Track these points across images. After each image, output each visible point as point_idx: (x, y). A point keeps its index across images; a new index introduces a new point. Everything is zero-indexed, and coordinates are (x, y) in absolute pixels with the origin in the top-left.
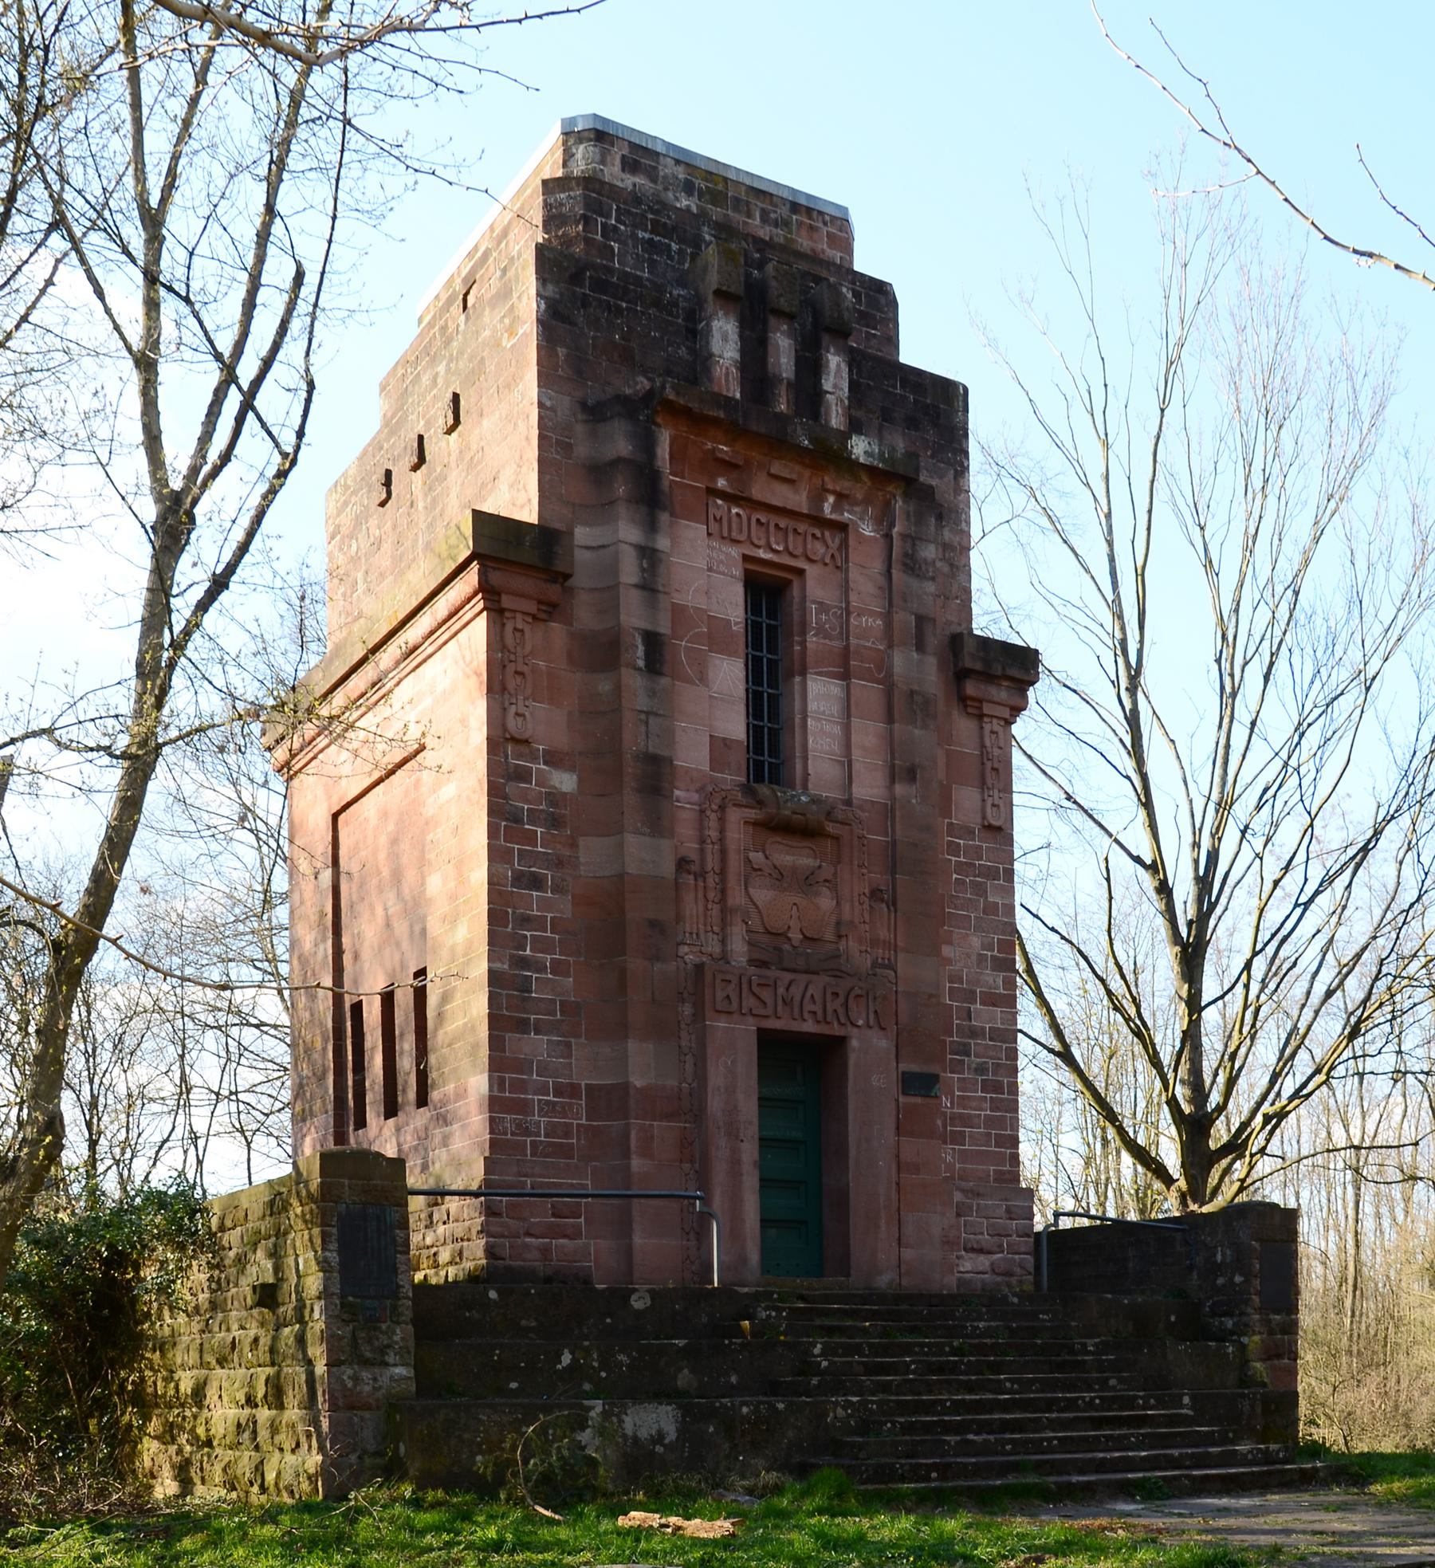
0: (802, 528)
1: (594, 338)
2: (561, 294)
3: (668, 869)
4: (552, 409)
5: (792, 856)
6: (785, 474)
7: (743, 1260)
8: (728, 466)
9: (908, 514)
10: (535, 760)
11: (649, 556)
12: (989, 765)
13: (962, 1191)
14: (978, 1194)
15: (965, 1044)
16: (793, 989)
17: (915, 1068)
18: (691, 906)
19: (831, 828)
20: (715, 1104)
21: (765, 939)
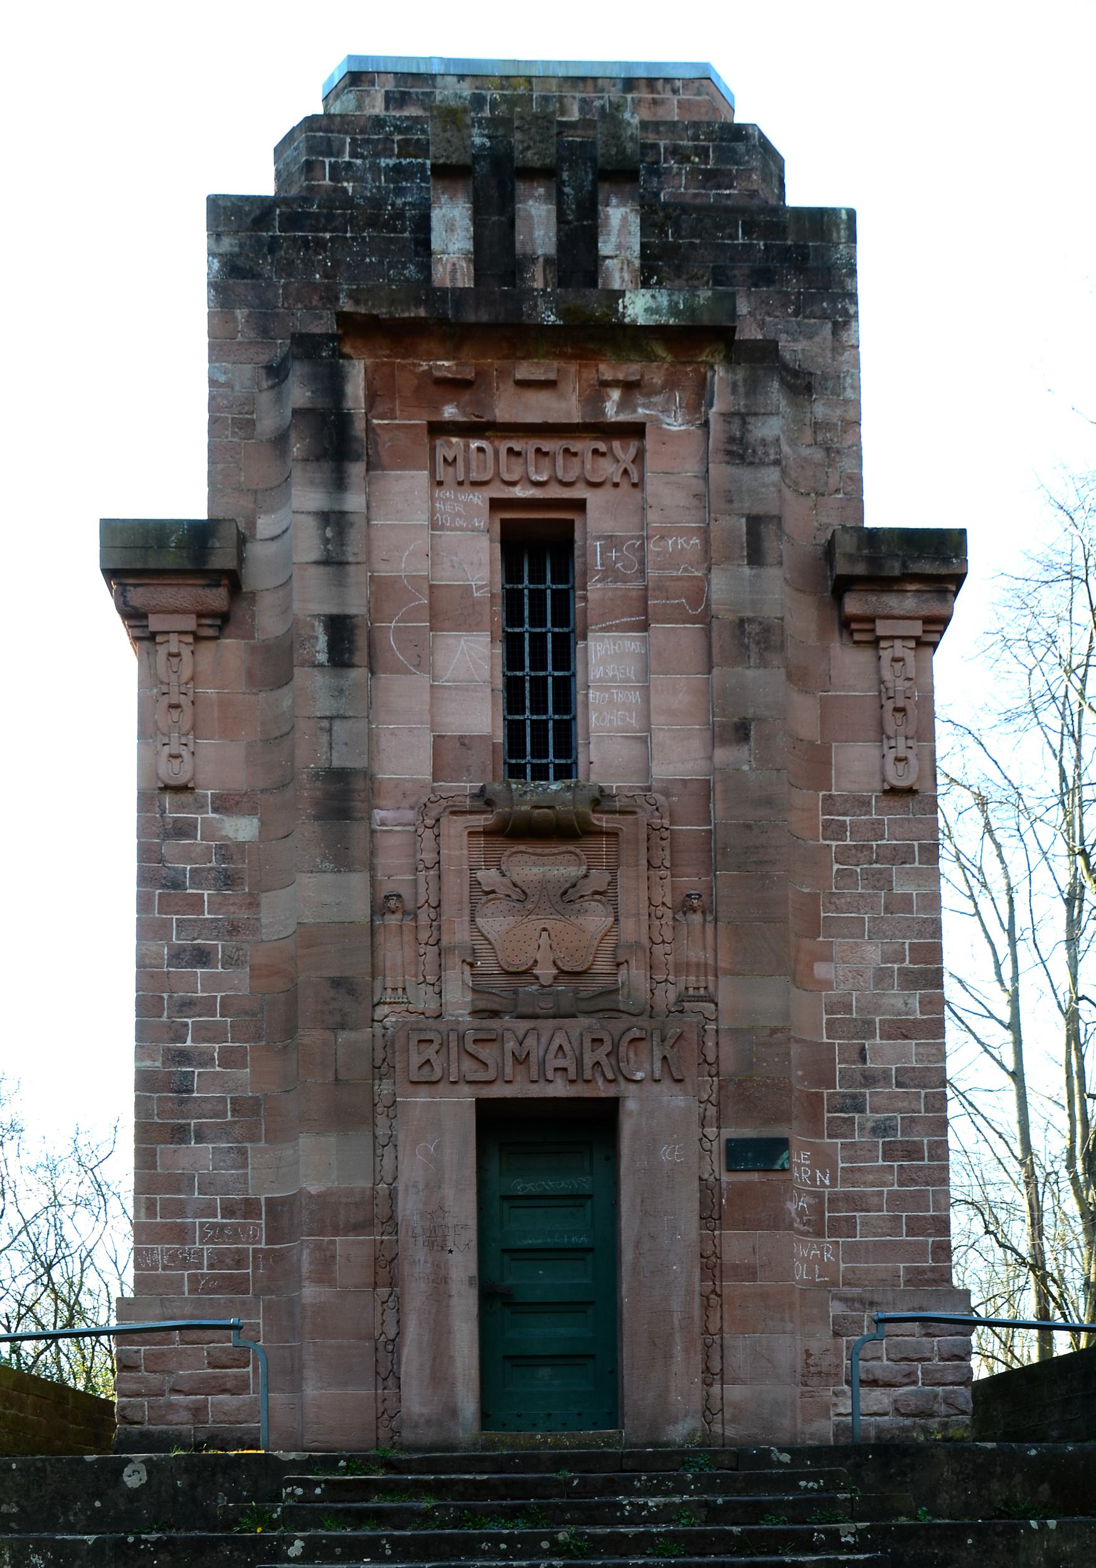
0: (576, 446)
1: (285, 286)
2: (241, 246)
3: (361, 910)
4: (228, 385)
5: (534, 867)
6: (539, 375)
7: (453, 1412)
8: (455, 386)
9: (734, 386)
10: (200, 807)
11: (334, 521)
12: (889, 705)
13: (845, 1300)
14: (872, 1304)
15: (854, 1097)
16: (531, 1041)
17: (748, 1132)
18: (395, 953)
19: (603, 821)
20: (409, 1207)
21: (502, 981)
